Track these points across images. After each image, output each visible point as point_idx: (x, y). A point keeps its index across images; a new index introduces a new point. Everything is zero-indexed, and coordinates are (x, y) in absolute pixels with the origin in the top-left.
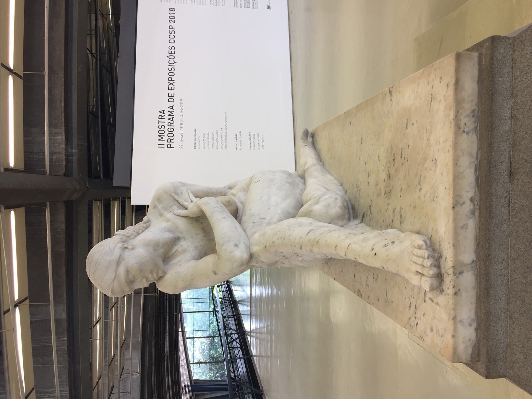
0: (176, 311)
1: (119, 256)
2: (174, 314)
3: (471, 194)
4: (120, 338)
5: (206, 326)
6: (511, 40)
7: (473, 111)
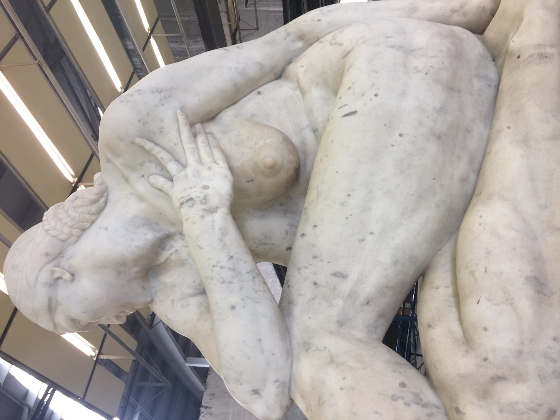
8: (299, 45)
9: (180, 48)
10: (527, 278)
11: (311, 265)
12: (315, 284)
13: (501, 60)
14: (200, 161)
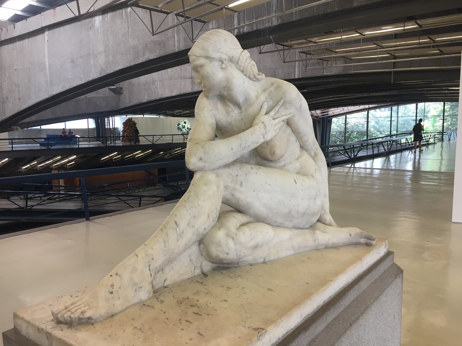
0: (390, 101)
1: (213, 57)
4: (348, 55)
5: (379, 128)
8: (313, 154)
9: (273, 5)
10: (258, 243)
11: (243, 173)
12: (237, 176)
13: (311, 229)
14: (276, 125)
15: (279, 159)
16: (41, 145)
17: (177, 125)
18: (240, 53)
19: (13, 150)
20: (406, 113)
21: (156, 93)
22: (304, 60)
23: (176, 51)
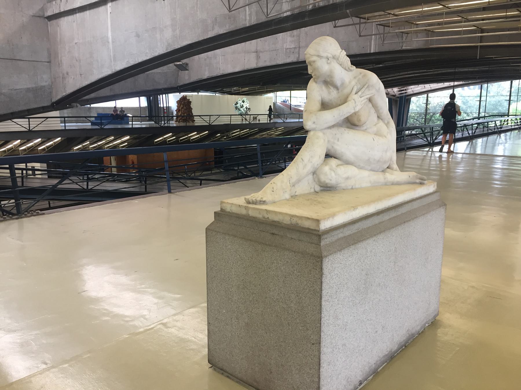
0: (479, 78)
2: (477, 75)
3: (270, 218)
5: (466, 109)
6: (319, 244)
7: (298, 224)
8: (386, 122)
12: (336, 134)
14: (362, 101)
15: (363, 125)
16: (93, 124)
17: (234, 105)
18: (340, 52)
19: (66, 129)
20: (499, 92)
21: (218, 69)
22: (381, 34)
23: (247, 26)
